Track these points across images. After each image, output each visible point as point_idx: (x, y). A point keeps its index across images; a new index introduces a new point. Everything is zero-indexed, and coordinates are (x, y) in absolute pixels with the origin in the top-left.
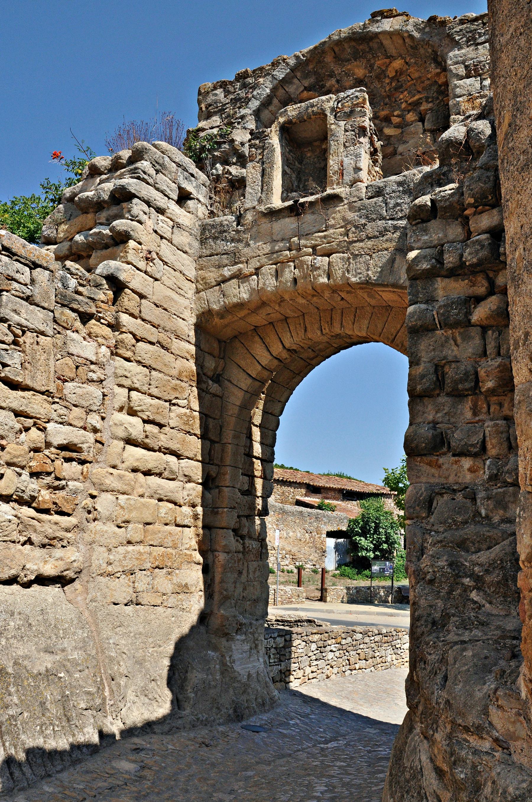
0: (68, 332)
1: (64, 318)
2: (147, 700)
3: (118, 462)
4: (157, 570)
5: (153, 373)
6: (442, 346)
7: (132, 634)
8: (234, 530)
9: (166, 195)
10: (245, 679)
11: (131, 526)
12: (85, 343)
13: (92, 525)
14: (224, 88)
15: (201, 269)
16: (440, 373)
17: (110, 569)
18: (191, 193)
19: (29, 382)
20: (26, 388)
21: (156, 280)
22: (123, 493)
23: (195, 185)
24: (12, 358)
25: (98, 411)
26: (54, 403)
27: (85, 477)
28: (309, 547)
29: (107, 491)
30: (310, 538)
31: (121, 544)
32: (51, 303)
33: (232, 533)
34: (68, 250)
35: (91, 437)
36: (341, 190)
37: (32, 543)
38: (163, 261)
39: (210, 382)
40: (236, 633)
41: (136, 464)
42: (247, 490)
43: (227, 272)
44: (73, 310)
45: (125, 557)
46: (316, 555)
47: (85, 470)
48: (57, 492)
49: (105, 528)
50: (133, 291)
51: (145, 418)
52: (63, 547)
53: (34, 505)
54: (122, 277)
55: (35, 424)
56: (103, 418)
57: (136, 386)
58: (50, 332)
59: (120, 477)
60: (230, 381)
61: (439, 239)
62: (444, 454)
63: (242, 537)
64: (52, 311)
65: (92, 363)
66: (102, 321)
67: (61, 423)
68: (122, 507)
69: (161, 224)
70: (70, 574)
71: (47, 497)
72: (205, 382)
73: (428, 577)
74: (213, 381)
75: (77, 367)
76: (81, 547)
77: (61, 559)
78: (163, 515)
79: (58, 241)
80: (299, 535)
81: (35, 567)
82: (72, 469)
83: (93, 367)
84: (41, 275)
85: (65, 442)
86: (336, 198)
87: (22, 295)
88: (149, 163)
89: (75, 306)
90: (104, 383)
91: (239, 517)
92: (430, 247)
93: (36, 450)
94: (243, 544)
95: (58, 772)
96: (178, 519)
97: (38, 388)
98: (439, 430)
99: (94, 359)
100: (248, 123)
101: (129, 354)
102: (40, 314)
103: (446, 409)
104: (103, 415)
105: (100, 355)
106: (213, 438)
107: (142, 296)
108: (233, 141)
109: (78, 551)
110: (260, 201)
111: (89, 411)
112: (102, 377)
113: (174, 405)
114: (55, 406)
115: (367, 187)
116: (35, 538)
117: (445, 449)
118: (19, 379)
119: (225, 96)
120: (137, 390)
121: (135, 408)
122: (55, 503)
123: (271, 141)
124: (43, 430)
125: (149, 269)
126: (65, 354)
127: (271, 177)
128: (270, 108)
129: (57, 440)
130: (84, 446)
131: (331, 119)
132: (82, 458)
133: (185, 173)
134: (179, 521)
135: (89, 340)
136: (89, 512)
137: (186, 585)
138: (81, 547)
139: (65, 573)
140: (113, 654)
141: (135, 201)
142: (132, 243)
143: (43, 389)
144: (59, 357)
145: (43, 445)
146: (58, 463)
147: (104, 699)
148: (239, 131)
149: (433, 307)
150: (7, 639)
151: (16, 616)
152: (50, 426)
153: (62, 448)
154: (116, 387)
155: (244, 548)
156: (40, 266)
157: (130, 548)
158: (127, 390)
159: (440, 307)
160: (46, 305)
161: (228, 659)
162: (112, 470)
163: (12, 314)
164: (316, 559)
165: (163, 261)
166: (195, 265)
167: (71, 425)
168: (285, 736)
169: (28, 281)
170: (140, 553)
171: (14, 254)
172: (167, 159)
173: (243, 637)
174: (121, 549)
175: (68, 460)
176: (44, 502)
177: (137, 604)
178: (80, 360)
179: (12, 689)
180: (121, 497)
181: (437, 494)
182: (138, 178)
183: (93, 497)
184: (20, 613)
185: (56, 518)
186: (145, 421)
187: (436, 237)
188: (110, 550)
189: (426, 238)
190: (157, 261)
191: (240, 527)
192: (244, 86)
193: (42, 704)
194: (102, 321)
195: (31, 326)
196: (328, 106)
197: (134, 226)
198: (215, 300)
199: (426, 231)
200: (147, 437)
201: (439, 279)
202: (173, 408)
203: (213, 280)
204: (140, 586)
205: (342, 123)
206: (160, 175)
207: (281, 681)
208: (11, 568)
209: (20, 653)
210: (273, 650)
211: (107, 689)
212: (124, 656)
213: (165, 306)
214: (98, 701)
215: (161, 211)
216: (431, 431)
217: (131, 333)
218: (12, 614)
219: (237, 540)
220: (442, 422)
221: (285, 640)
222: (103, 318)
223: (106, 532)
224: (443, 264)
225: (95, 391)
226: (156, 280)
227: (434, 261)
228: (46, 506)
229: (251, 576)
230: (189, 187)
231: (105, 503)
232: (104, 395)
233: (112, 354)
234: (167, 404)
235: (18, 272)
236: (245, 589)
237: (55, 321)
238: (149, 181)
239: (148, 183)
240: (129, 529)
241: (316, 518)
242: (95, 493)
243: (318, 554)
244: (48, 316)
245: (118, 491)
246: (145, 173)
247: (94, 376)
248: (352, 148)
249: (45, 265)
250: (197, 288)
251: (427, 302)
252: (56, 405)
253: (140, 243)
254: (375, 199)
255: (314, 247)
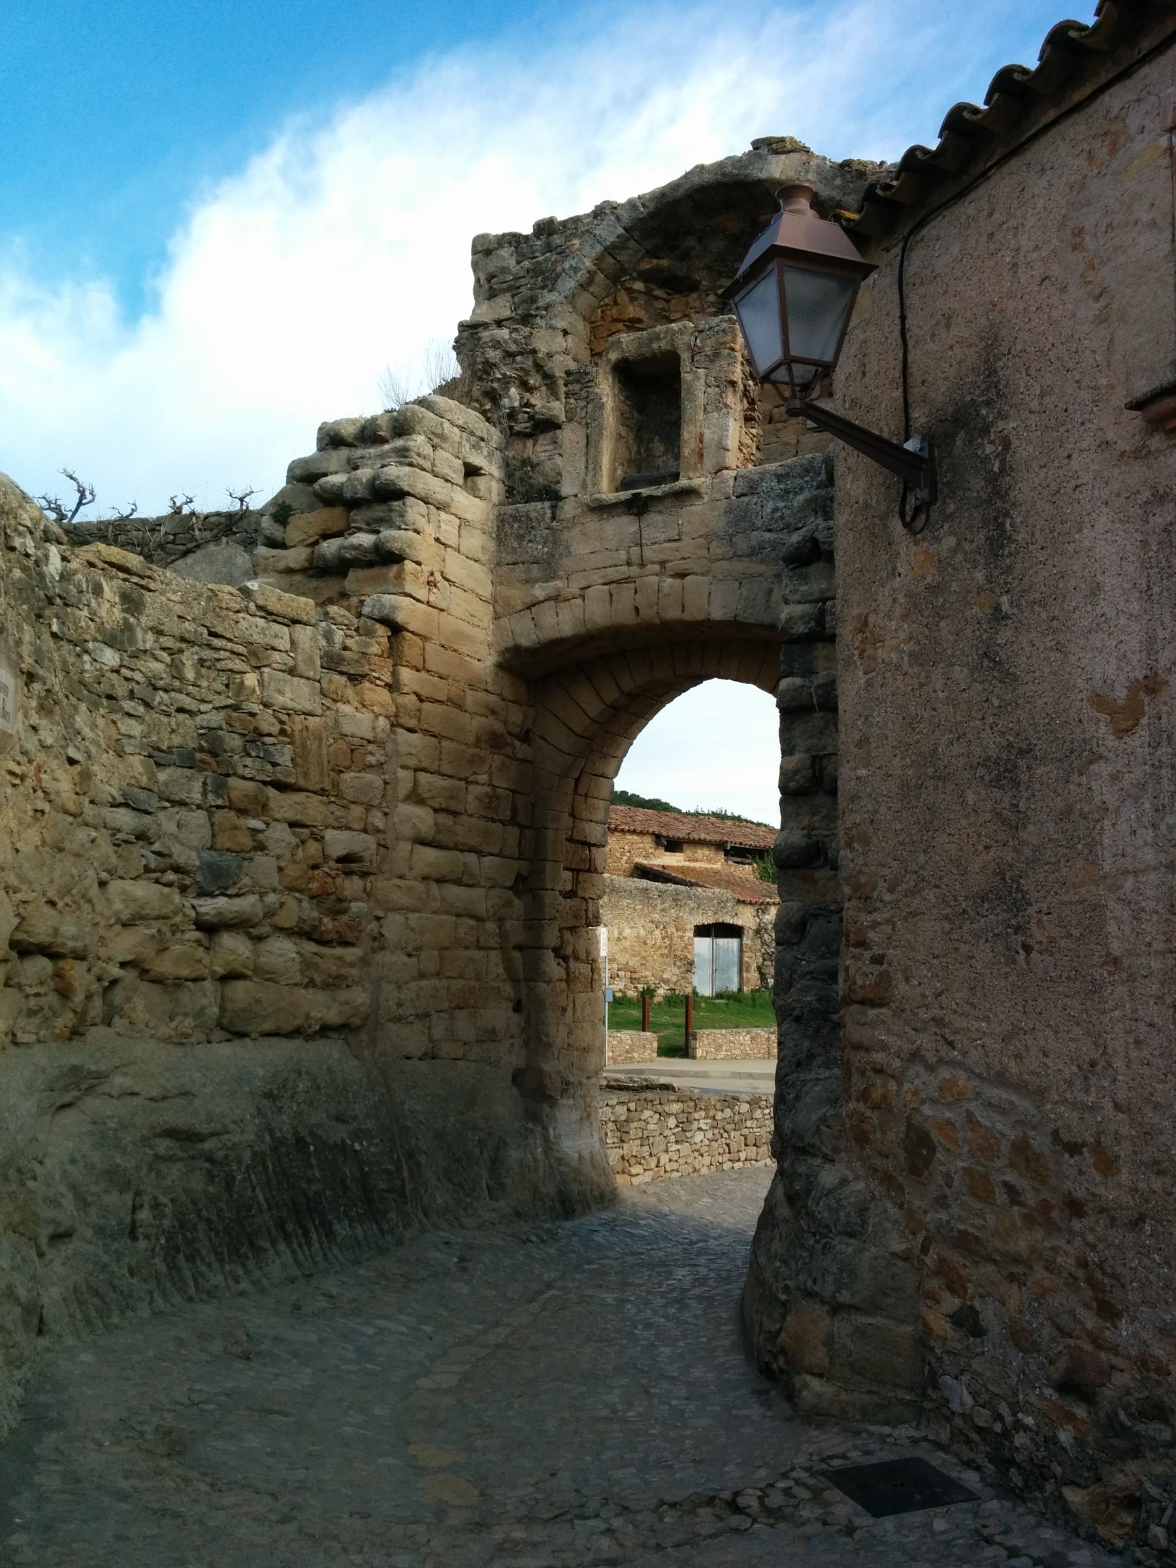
0: (339, 704)
1: (333, 687)
2: (450, 1186)
3: (405, 870)
4: (457, 1011)
5: (444, 743)
6: (821, 733)
7: (429, 1098)
8: (555, 950)
9: (447, 481)
10: (575, 1163)
11: (424, 954)
12: (358, 715)
13: (378, 957)
14: (516, 248)
15: (501, 584)
16: (817, 767)
17: (401, 1011)
18: (481, 468)
19: (302, 783)
20: (300, 790)
21: (442, 610)
22: (413, 911)
23: (485, 453)
24: (282, 754)
25: (379, 807)
26: (330, 802)
27: (368, 894)
28: (662, 955)
29: (394, 910)
30: (663, 939)
31: (414, 979)
32: (316, 671)
33: (552, 954)
34: (307, 560)
35: (370, 841)
36: (699, 481)
37: (315, 986)
38: (448, 580)
39: (517, 743)
40: (562, 1097)
41: (427, 871)
42: (571, 891)
43: (539, 591)
44: (341, 673)
45: (418, 995)
46: (676, 971)
47: (368, 884)
48: (338, 917)
49: (394, 958)
50: (413, 633)
51: (437, 806)
52: (348, 986)
53: (315, 936)
54: (400, 618)
55: (312, 833)
56: (386, 814)
57: (424, 765)
58: (319, 711)
59: (410, 889)
60: (543, 739)
61: (822, 591)
62: (822, 867)
63: (566, 959)
64: (319, 681)
65: (369, 741)
66: (378, 682)
67: (339, 828)
68: (413, 930)
69: (444, 527)
70: (356, 1021)
71: (330, 926)
72: (510, 745)
73: (796, 1013)
74: (520, 740)
75: (352, 751)
76: (367, 985)
77: (347, 1003)
78: (462, 935)
79: (289, 543)
80: (642, 933)
81: (319, 1015)
82: (355, 885)
83: (370, 747)
84: (304, 634)
85: (345, 852)
86: (690, 493)
87: (284, 668)
88: (423, 437)
89: (344, 669)
90: (385, 767)
91: (560, 930)
92: (810, 602)
93: (315, 867)
94: (567, 969)
95: (368, 1260)
96: (482, 940)
97: (312, 788)
98: (814, 839)
99: (370, 736)
100: (558, 319)
101: (412, 723)
102: (303, 687)
103: (825, 812)
104: (387, 810)
105: (379, 730)
106: (523, 822)
107: (424, 638)
108: (534, 352)
109: (364, 991)
110: (584, 486)
111: (369, 808)
112: (383, 759)
113: (472, 782)
114: (333, 807)
115: (735, 478)
116: (318, 979)
117: (821, 862)
118: (292, 780)
119: (518, 262)
120: (424, 770)
121: (424, 796)
122: (338, 932)
123: (597, 390)
124: (320, 839)
125: (432, 599)
126: (337, 736)
127: (598, 452)
128: (591, 289)
129: (337, 851)
130: (366, 854)
131: (686, 365)
132: (365, 869)
133: (472, 438)
134: (482, 943)
135: (364, 710)
136: (374, 939)
137: (493, 1031)
138: (367, 985)
139: (351, 1020)
140: (409, 1124)
141: (410, 500)
142: (409, 565)
143: (317, 787)
144: (332, 741)
145: (321, 860)
146: (339, 880)
147: (403, 1180)
148: (543, 332)
149: (811, 682)
150: (299, 1104)
151: (305, 1077)
152: (330, 834)
153: (340, 860)
154: (399, 770)
155: (568, 974)
156: (299, 622)
157: (424, 983)
158: (412, 772)
159: (818, 686)
160: (311, 674)
161: (551, 1131)
162: (399, 882)
163: (276, 696)
164: (674, 979)
165: (448, 580)
166: (491, 577)
167: (350, 829)
168: (634, 1235)
169: (288, 647)
170: (436, 989)
171: (270, 614)
172: (447, 425)
173: (571, 1102)
174: (413, 986)
175: (349, 874)
176: (327, 932)
177: (433, 1058)
178: (356, 741)
179: (314, 1162)
180: (411, 916)
181: (811, 915)
182: (411, 465)
183: (378, 918)
184: (307, 1073)
185: (339, 951)
186: (436, 810)
187: (817, 590)
188: (399, 987)
189: (805, 588)
190: (442, 583)
191: (562, 944)
192: (549, 248)
193: (343, 1181)
194: (378, 682)
195: (298, 707)
196: (682, 342)
197: (411, 540)
198: (526, 634)
199: (805, 579)
200: (439, 831)
201: (820, 645)
202: (471, 788)
203: (518, 602)
204: (438, 1032)
205: (701, 371)
206: (440, 452)
207: (624, 1172)
208: (295, 1018)
209: (313, 1121)
210: (611, 1126)
211: (405, 1169)
212: (422, 1127)
213: (455, 647)
214: (398, 1183)
215: (441, 507)
216: (805, 840)
217: (415, 693)
218: (300, 1075)
219: (559, 964)
220: (819, 828)
221: (629, 1110)
222: (378, 679)
223: (395, 963)
224: (823, 626)
225: (373, 779)
226: (442, 610)
227: (813, 623)
228: (329, 937)
229: (578, 1014)
230: (477, 460)
231: (393, 926)
232: (386, 783)
233: (392, 725)
234: (463, 782)
235: (276, 636)
236: (570, 1033)
237: (323, 693)
238: (425, 466)
239: (423, 469)
240: (422, 958)
241: (674, 900)
242: (381, 914)
243: (680, 967)
244: (314, 688)
245: (407, 908)
246: (419, 455)
247: (372, 760)
248: (715, 414)
249: (305, 618)
250: (495, 611)
251: (803, 675)
252: (332, 805)
253: (419, 563)
254: (746, 499)
255: (662, 563)
